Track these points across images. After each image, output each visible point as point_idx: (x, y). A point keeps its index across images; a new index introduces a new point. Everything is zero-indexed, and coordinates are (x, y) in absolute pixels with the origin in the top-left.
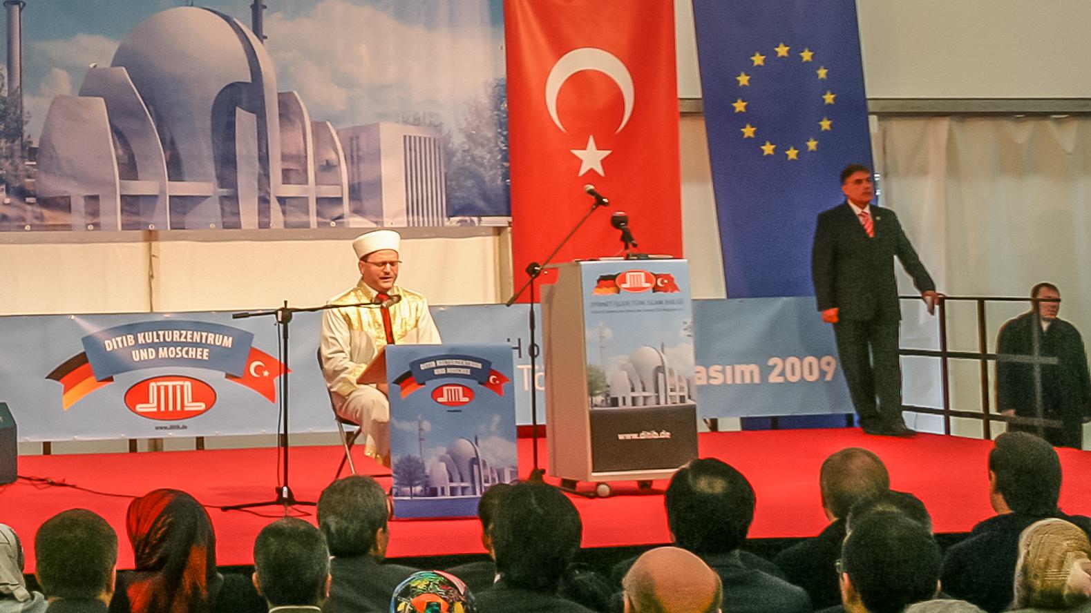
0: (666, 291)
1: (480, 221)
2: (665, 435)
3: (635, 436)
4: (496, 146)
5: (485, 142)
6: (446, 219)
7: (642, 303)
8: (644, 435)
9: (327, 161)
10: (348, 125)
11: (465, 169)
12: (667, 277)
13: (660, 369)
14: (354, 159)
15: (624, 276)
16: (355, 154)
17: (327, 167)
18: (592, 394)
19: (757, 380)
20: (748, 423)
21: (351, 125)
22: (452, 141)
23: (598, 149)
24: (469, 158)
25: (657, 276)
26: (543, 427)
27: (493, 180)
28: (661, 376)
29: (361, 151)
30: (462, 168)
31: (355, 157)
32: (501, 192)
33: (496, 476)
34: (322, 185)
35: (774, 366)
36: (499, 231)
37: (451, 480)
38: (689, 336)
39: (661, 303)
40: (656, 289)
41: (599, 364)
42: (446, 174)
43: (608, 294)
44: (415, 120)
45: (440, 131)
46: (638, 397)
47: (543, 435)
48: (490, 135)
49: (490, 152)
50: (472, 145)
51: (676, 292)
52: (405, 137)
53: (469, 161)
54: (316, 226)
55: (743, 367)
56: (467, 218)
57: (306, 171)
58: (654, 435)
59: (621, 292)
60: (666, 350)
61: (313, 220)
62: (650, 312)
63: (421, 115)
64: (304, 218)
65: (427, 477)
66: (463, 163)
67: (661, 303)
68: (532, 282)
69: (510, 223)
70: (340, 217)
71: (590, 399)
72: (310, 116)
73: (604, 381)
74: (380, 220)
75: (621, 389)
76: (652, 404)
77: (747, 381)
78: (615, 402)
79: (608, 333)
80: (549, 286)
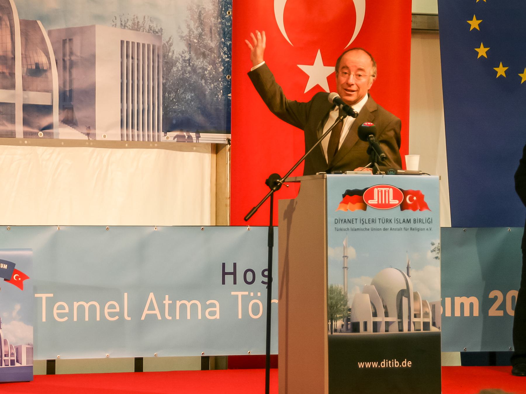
0: (414, 209)
1: (198, 137)
2: (407, 364)
3: (375, 365)
4: (219, 57)
5: (207, 52)
6: (162, 134)
7: (389, 221)
8: (384, 364)
9: (37, 65)
10: (60, 25)
11: (184, 80)
12: (417, 193)
13: (404, 293)
14: (66, 65)
15: (372, 191)
16: (67, 58)
17: (36, 71)
18: (332, 318)
19: (476, 313)
20: (466, 357)
21: (64, 26)
22: (172, 48)
23: (312, 64)
24: (189, 68)
25: (406, 193)
26: (276, 357)
27: (214, 93)
28: (405, 300)
29: (73, 55)
30: (181, 79)
31: (68, 63)
32: (221, 107)
33: (14, 351)
34: (30, 90)
35: (496, 298)
36: (216, 148)
37: (375, 315)
38: (437, 258)
39: (409, 221)
40: (404, 206)
41: (340, 286)
42: (164, 85)
43: (353, 211)
44: (134, 24)
45: (160, 38)
46: (380, 322)
47: (276, 366)
48: (213, 44)
49: (213, 63)
50: (193, 54)
51: (425, 211)
52: (122, 42)
53: (189, 72)
54: (22, 136)
55: (464, 299)
56: (185, 134)
57: (12, 75)
58: (396, 364)
59: (368, 208)
60: (412, 272)
61: (19, 128)
62: (397, 232)
63: (141, 21)
64: (9, 127)
65: (350, 310)
66: (183, 74)
67: (409, 221)
68: (272, 195)
69: (229, 140)
70: (50, 127)
71: (330, 323)
72: (19, 14)
73: (345, 305)
74: (92, 132)
75: (362, 313)
76: (394, 330)
77: (467, 314)
78: (355, 327)
79: (351, 252)
80: (288, 201)
